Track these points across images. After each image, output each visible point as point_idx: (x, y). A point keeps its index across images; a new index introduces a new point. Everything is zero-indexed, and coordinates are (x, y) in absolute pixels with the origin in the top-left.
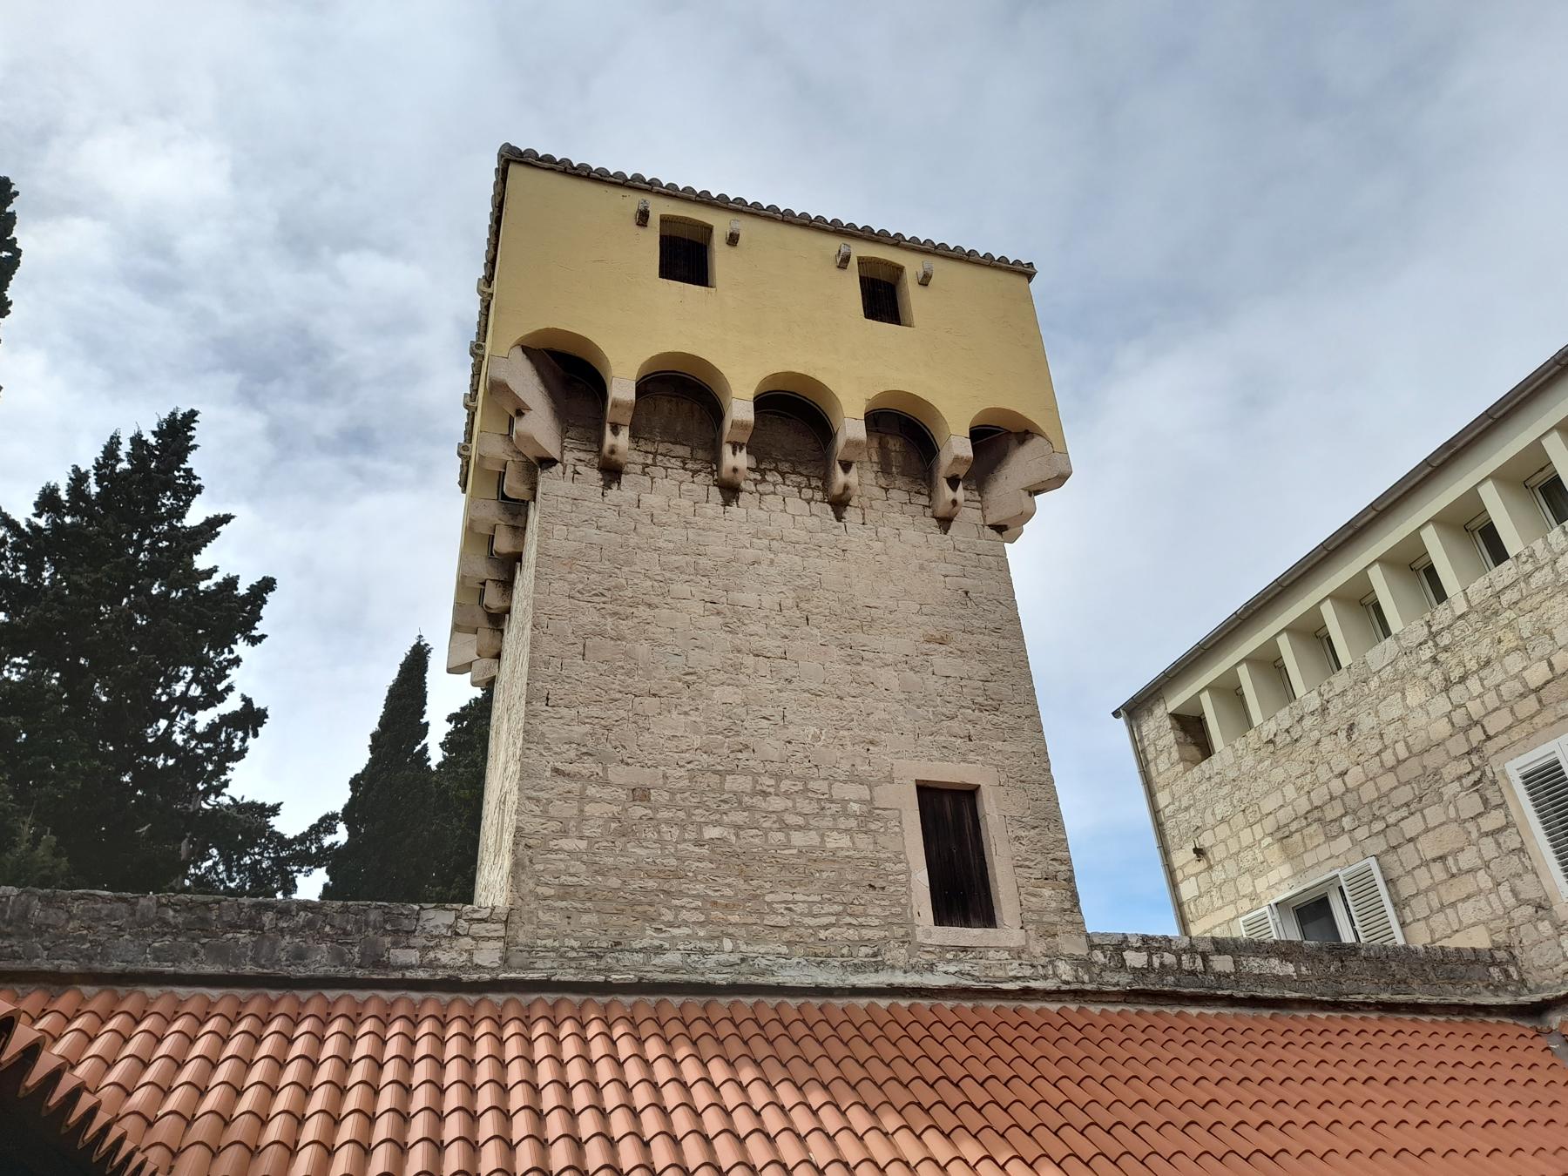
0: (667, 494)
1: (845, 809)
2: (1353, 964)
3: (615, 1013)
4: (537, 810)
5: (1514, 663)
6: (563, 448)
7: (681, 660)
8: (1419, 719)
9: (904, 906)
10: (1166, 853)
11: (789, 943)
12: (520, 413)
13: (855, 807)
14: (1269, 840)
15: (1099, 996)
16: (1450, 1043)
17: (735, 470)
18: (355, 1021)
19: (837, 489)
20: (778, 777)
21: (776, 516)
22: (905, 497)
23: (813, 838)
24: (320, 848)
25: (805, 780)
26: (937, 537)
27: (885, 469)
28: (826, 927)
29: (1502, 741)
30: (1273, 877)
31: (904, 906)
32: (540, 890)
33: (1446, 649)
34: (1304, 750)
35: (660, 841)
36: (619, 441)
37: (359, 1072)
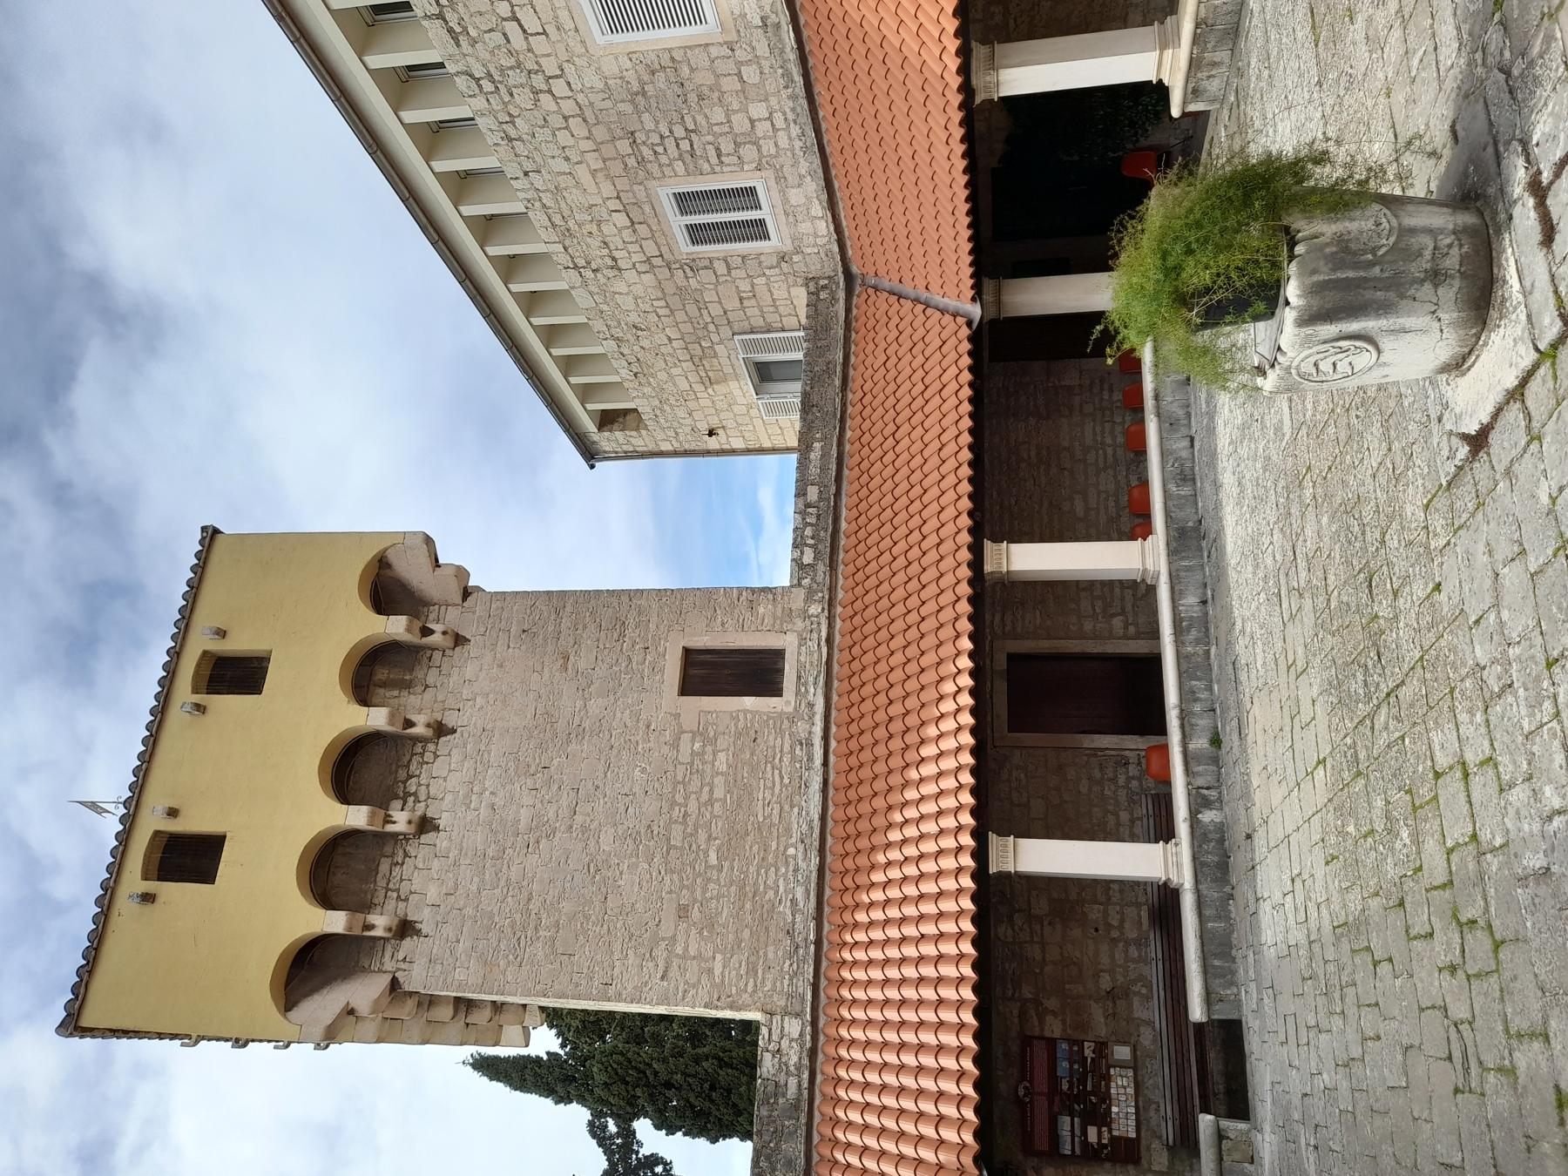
0: (424, 882)
1: (698, 754)
2: (815, 399)
3: (836, 938)
4: (692, 992)
5: (607, 229)
6: (380, 971)
7: (577, 875)
8: (638, 290)
9: (769, 718)
10: (708, 453)
11: (792, 807)
12: (351, 1012)
13: (697, 745)
14: (710, 391)
15: (832, 589)
16: (868, 359)
17: (410, 822)
18: (836, 1122)
19: (429, 733)
20: (673, 803)
21: (450, 785)
22: (434, 671)
23: (719, 781)
24: (618, 1135)
25: (675, 783)
26: (472, 649)
27: (407, 686)
28: (782, 778)
29: (665, 250)
30: (737, 392)
31: (769, 718)
32: (750, 989)
33: (589, 263)
34: (648, 357)
35: (718, 897)
36: (381, 922)
37: (872, 1119)
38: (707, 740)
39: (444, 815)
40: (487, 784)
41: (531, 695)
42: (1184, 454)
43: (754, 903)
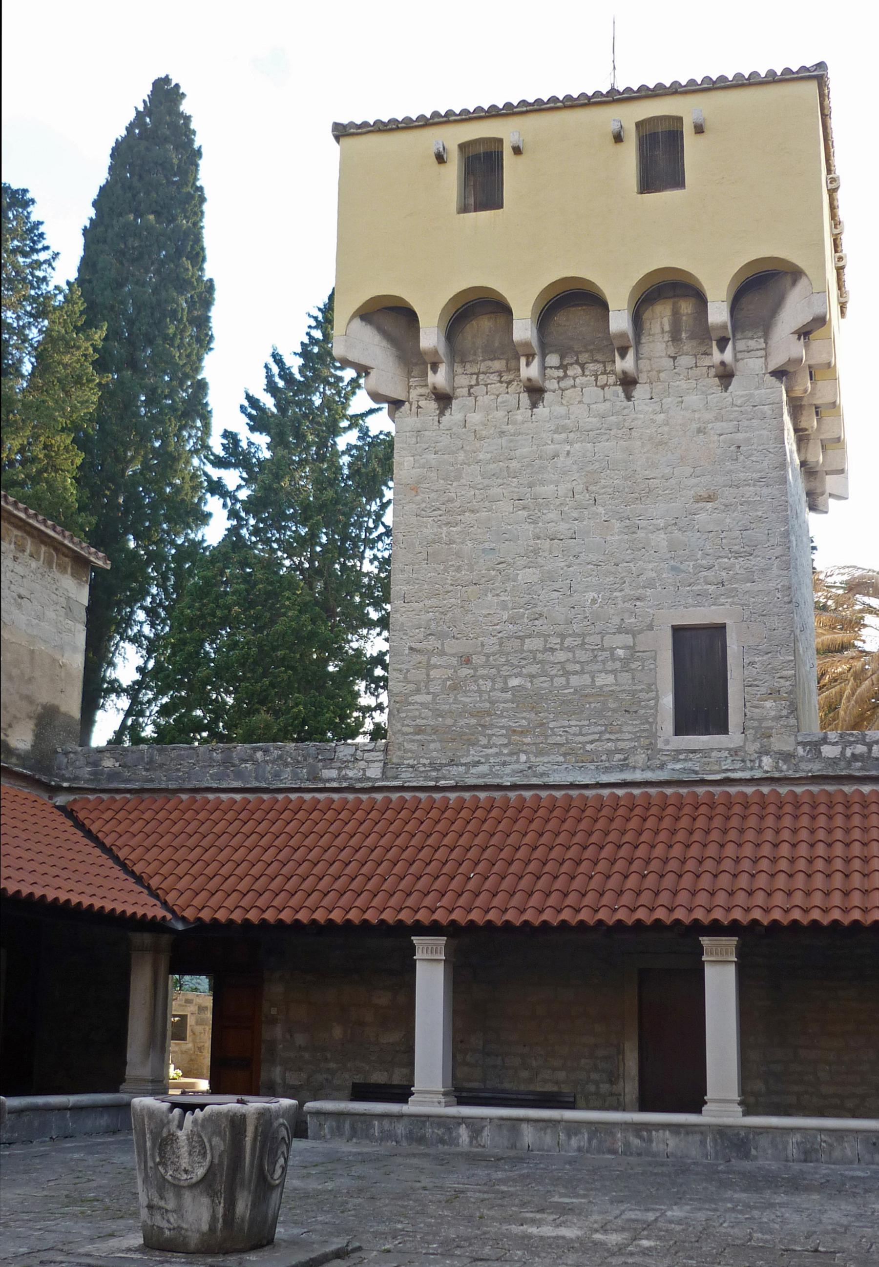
0: (487, 405)
1: (612, 654)
11: (565, 755)
20: (563, 637)
23: (586, 679)
25: (583, 635)
26: (717, 396)
28: (592, 742)
31: (651, 724)
38: (626, 663)
39: (547, 410)
40: (577, 446)
41: (668, 470)
42: (837, 1154)
43: (475, 726)
